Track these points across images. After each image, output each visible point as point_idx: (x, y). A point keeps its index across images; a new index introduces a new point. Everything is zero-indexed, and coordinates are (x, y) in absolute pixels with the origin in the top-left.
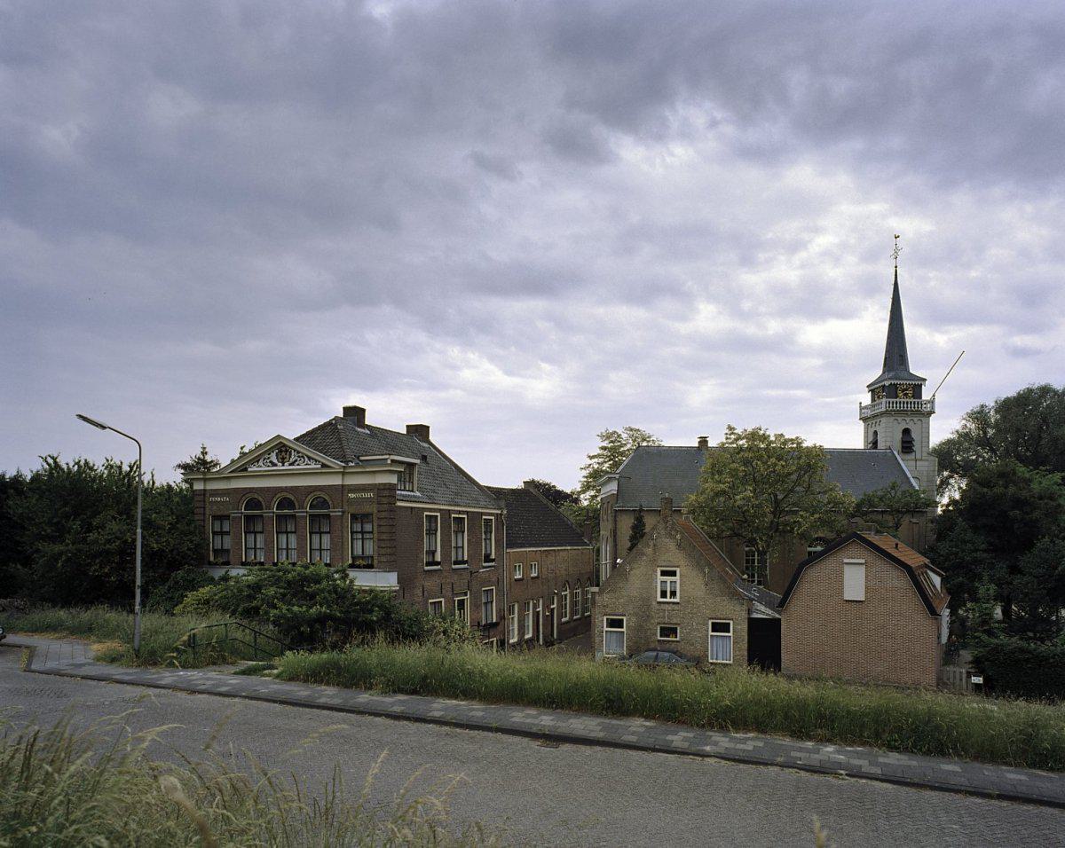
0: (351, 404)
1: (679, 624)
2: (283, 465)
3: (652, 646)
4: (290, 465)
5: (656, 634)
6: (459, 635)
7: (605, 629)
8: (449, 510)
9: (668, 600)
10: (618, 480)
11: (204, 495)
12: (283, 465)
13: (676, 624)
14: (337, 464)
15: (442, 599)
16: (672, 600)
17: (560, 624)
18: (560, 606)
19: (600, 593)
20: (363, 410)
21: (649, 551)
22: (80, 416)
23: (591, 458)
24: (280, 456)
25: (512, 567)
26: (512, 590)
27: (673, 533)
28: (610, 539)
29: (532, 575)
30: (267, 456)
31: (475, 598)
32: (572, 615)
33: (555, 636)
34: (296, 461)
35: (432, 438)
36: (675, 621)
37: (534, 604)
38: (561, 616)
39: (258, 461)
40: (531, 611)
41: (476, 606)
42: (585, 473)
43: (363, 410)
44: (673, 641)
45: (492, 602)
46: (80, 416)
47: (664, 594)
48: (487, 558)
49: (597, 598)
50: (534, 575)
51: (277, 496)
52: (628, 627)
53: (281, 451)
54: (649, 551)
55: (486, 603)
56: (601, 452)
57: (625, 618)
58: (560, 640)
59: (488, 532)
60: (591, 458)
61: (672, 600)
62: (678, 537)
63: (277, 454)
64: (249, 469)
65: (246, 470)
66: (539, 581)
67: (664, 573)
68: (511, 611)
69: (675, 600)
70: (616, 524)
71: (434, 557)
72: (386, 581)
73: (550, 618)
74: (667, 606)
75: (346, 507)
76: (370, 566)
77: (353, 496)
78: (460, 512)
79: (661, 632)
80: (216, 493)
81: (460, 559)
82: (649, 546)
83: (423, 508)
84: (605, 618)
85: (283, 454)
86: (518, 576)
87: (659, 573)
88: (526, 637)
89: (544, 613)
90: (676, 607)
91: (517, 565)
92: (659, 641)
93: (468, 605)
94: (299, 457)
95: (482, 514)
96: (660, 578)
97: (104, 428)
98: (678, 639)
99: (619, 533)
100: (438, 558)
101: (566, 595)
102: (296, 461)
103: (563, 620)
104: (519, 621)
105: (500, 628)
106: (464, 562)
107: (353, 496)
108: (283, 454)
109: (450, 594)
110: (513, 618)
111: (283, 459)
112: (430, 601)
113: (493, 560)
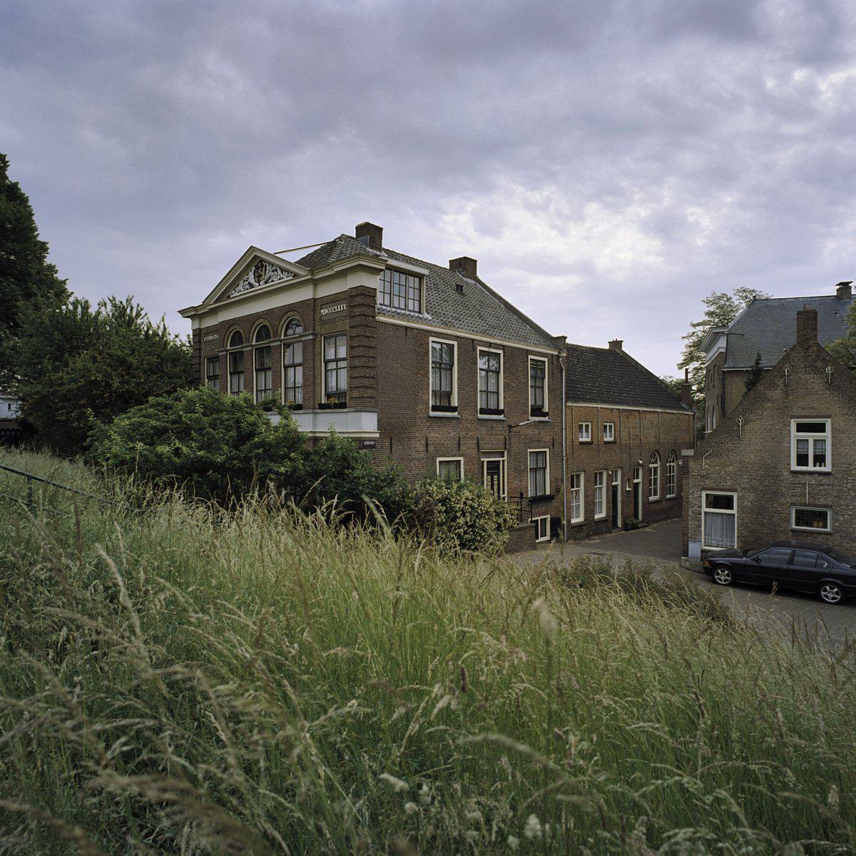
0: (362, 221)
1: (830, 507)
3: (782, 538)
4: (266, 282)
5: (788, 521)
6: (471, 507)
7: (704, 509)
8: (473, 340)
9: (811, 468)
10: (727, 334)
13: (824, 506)
15: (461, 459)
16: (818, 469)
17: (647, 504)
18: (647, 481)
19: (697, 457)
20: (381, 229)
21: (777, 394)
23: (694, 326)
25: (575, 427)
26: (575, 455)
27: (819, 364)
28: (716, 407)
29: (606, 439)
31: (518, 460)
32: (663, 495)
33: (640, 518)
35: (480, 275)
36: (822, 501)
37: (609, 476)
38: (648, 493)
40: (604, 485)
41: (518, 471)
42: (687, 342)
43: (381, 229)
44: (820, 533)
45: (545, 468)
47: (802, 460)
48: (537, 411)
49: (691, 464)
50: (608, 439)
51: (255, 325)
52: (741, 508)
54: (777, 394)
55: (534, 470)
56: (707, 318)
57: (735, 496)
58: (647, 522)
59: (538, 377)
60: (694, 326)
61: (818, 469)
62: (829, 369)
66: (616, 447)
67: (801, 428)
68: (574, 481)
69: (823, 469)
70: (724, 388)
71: (449, 402)
72: (367, 424)
74: (808, 477)
75: (318, 328)
76: (343, 406)
77: (326, 311)
78: (490, 345)
79: (797, 517)
81: (492, 406)
82: (775, 386)
83: (428, 331)
84: (704, 494)
86: (585, 438)
87: (793, 427)
88: (597, 517)
90: (825, 480)
91: (584, 424)
92: (793, 531)
93: (505, 471)
95: (528, 352)
96: (795, 435)
98: (828, 529)
99: (728, 398)
100: (455, 403)
101: (655, 469)
103: (652, 498)
104: (586, 496)
105: (555, 503)
106: (499, 412)
107: (326, 311)
108: (259, 271)
109: (474, 452)
110: (577, 492)
111: (260, 276)
112: (439, 459)
113: (545, 415)
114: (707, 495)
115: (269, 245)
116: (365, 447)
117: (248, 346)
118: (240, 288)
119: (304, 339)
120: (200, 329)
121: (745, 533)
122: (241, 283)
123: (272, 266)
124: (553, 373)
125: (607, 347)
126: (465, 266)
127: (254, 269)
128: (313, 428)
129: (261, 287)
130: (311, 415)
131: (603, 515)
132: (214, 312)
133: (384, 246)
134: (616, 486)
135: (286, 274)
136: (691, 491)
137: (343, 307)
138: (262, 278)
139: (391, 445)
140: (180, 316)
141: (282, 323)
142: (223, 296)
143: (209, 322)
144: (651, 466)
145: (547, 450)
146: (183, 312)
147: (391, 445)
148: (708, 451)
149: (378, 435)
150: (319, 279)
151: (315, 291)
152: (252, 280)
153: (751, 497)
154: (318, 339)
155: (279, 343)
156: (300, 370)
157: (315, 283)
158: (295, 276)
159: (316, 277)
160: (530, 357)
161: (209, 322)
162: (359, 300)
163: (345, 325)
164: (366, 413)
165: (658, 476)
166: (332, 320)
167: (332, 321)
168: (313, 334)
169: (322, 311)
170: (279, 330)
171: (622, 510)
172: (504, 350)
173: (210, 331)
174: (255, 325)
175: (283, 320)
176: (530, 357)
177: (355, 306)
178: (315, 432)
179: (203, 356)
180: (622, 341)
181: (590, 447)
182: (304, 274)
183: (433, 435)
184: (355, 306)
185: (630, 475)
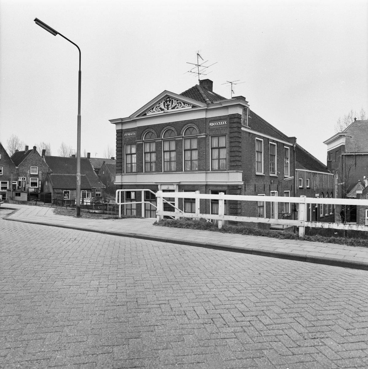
2: (168, 109)
4: (172, 109)
11: (122, 133)
12: (168, 109)
14: (202, 106)
22: (37, 21)
24: (166, 104)
30: (158, 105)
34: (176, 106)
39: (153, 109)
46: (37, 21)
51: (164, 129)
53: (167, 101)
63: (164, 104)
64: (147, 114)
65: (145, 114)
73: (315, 213)
75: (208, 132)
77: (213, 124)
80: (128, 130)
85: (168, 102)
89: (312, 210)
94: (178, 103)
97: (55, 33)
102: (176, 106)
107: (213, 124)
108: (168, 102)
111: (168, 105)
128: (206, 180)
130: (205, 174)
136: (361, 210)
141: (183, 129)
145: (289, 191)
146: (109, 120)
163: (227, 132)
164: (138, 175)
165: (322, 210)
166: (217, 129)
168: (205, 135)
169: (210, 124)
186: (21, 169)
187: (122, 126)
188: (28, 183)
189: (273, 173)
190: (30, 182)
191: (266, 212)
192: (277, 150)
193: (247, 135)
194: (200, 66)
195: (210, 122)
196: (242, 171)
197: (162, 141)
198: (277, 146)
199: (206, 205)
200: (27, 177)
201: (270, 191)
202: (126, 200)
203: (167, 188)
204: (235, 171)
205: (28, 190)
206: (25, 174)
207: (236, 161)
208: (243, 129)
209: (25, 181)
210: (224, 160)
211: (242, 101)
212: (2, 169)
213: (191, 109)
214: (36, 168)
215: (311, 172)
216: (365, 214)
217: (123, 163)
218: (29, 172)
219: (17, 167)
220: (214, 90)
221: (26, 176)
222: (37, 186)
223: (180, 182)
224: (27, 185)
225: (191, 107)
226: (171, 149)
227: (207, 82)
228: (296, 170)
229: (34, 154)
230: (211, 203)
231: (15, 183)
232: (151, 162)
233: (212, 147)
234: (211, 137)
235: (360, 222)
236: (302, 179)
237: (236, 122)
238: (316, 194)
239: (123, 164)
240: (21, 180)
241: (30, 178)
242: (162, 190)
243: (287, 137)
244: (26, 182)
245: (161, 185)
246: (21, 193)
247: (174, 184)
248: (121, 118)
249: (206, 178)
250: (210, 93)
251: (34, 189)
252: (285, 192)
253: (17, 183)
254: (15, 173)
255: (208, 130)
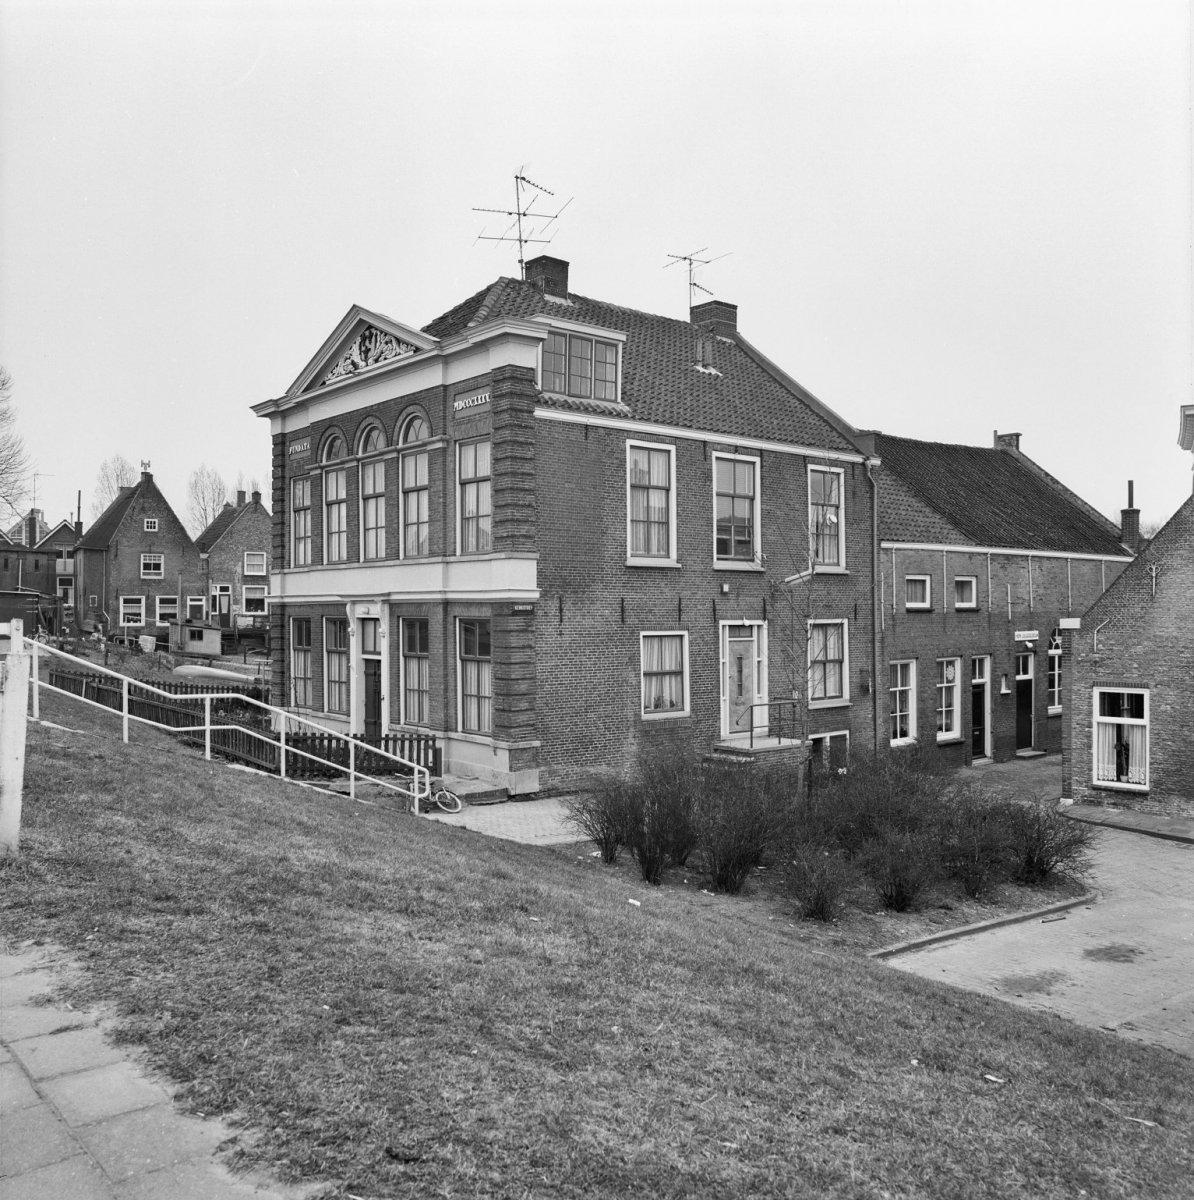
4: (376, 361)
8: (705, 443)
51: (362, 426)
57: (1146, 693)
64: (327, 383)
75: (450, 431)
88: (942, 736)
111: (368, 350)
112: (643, 633)
114: (1103, 695)
115: (378, 304)
116: (516, 613)
117: (352, 460)
118: (340, 369)
119: (347, 466)
120: (283, 435)
121: (1160, 756)
122: (341, 362)
123: (386, 335)
124: (854, 493)
125: (988, 443)
126: (717, 317)
127: (359, 340)
129: (368, 368)
130: (441, 566)
131: (955, 734)
132: (302, 406)
133: (571, 289)
134: (981, 686)
135: (403, 347)
137: (484, 396)
138: (370, 354)
139: (561, 610)
140: (254, 414)
141: (398, 424)
142: (315, 381)
143: (296, 423)
144: (1052, 652)
147: (561, 610)
148: (1102, 621)
149: (537, 595)
150: (287, 409)
151: (445, 375)
152: (357, 358)
153: (1172, 695)
154: (451, 448)
155: (355, 463)
156: (425, 496)
157: (446, 360)
158: (417, 350)
159: (282, 408)
160: (810, 467)
161: (296, 423)
162: (506, 387)
167: (469, 420)
168: (442, 440)
169: (456, 404)
170: (396, 434)
171: (993, 727)
172: (761, 456)
173: (298, 435)
174: (362, 426)
175: (401, 418)
176: (810, 467)
177: (502, 396)
178: (445, 592)
179: (287, 476)
180: (1018, 436)
181: (972, 617)
182: (428, 344)
183: (632, 595)
184: (502, 396)
185: (1008, 667)
186: (216, 560)
187: (283, 424)
188: (237, 602)
189: (738, 557)
190: (244, 598)
191: (693, 694)
192: (762, 479)
193: (579, 435)
194: (525, 215)
195: (457, 397)
196: (537, 555)
197: (358, 466)
198: (762, 467)
199: (446, 667)
200: (234, 584)
201: (716, 621)
202: (405, 657)
203: (364, 613)
204: (503, 555)
205: (235, 622)
206: (229, 575)
207: (507, 521)
208: (540, 413)
209: (229, 595)
210: (642, 525)
211: (509, 321)
212: (162, 562)
213: (411, 357)
214: (259, 558)
215: (942, 551)
216: (1090, 705)
217: (287, 536)
218: (239, 570)
219: (204, 556)
220: (573, 288)
221: (231, 580)
222: (263, 610)
223: (389, 594)
224: (234, 607)
225: (412, 353)
226: (739, 491)
227: (544, 266)
228: (884, 545)
229: (255, 515)
230: (461, 659)
231: (201, 600)
232: (305, 537)
233: (463, 477)
234: (460, 446)
235: (1074, 733)
236: (928, 578)
237: (507, 393)
238: (1017, 633)
239: (286, 539)
240: (217, 593)
241: (244, 587)
242: (358, 618)
243: (848, 429)
244: (232, 597)
245: (354, 603)
246: (205, 631)
247: (376, 599)
248: (271, 400)
249: (446, 578)
250: (559, 300)
251: (252, 619)
252: (815, 626)
253: (203, 603)
254: (200, 572)
255: (452, 424)
